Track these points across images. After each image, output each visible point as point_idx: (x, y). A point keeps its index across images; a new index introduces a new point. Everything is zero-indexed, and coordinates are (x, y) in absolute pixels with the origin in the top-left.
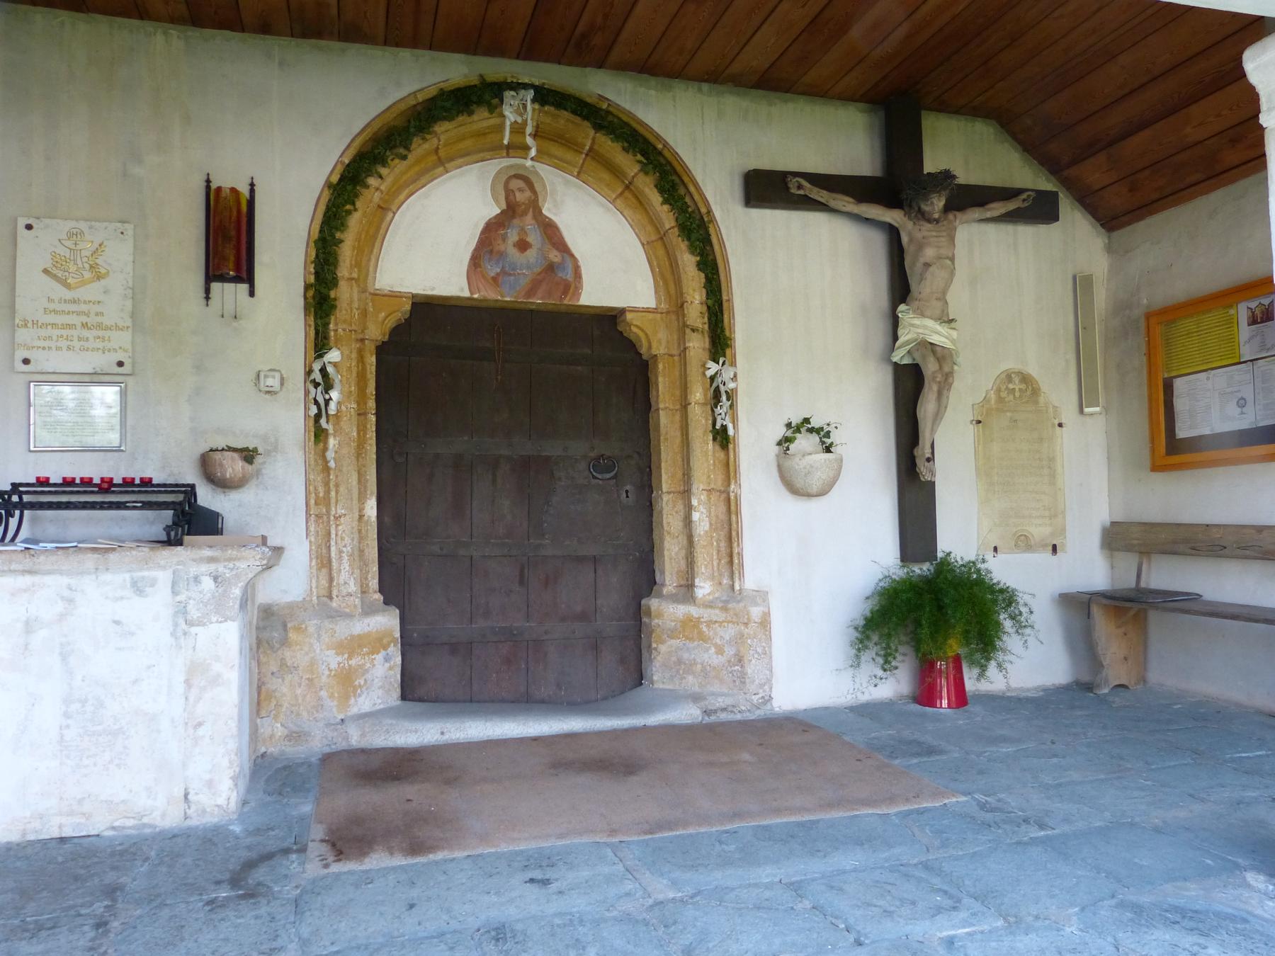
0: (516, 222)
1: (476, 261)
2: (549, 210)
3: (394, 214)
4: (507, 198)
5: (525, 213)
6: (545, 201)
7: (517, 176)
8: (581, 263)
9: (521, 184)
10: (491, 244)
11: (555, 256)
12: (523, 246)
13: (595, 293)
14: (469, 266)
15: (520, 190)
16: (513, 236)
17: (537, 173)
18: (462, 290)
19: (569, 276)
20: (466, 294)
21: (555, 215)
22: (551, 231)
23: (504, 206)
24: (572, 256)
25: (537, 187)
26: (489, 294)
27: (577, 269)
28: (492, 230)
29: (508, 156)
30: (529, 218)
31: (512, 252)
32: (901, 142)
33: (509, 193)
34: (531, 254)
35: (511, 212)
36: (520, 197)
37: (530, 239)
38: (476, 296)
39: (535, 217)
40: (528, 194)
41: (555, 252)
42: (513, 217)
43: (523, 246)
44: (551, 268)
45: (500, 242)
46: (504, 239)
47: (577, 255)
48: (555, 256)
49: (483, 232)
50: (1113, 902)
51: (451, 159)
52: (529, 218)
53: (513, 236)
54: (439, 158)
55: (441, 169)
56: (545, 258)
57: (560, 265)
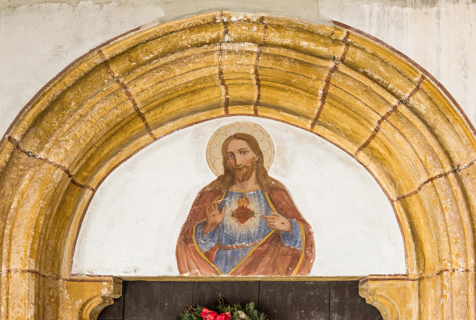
0: (235, 188)
1: (186, 237)
2: (276, 171)
3: (94, 191)
4: (225, 163)
5: (246, 178)
6: (270, 160)
7: (237, 137)
8: (313, 229)
9: (243, 144)
10: (205, 215)
11: (281, 223)
12: (243, 215)
13: (326, 265)
14: (179, 242)
15: (242, 151)
16: (232, 205)
17: (262, 131)
18: (170, 269)
19: (300, 247)
20: (175, 273)
21: (283, 176)
22: (277, 197)
23: (221, 172)
24: (303, 221)
25: (263, 146)
26: (202, 273)
27: (309, 235)
28: (207, 200)
29: (227, 114)
30: (251, 185)
31: (231, 223)
32: (227, 111)
33: (228, 155)
34: (253, 224)
35: (231, 175)
36: (240, 159)
37: (253, 206)
38: (186, 275)
39: (258, 181)
40: (251, 155)
41: (283, 219)
42: (232, 183)
43: (243, 215)
44: (278, 237)
45: (216, 212)
46: (221, 208)
47: (305, 216)
48: (281, 223)
49: (196, 203)
50: (20, 298)
51: (160, 124)
52: (251, 185)
53: (232, 205)
54: (147, 124)
55: (147, 136)
56: (269, 227)
57: (289, 234)
